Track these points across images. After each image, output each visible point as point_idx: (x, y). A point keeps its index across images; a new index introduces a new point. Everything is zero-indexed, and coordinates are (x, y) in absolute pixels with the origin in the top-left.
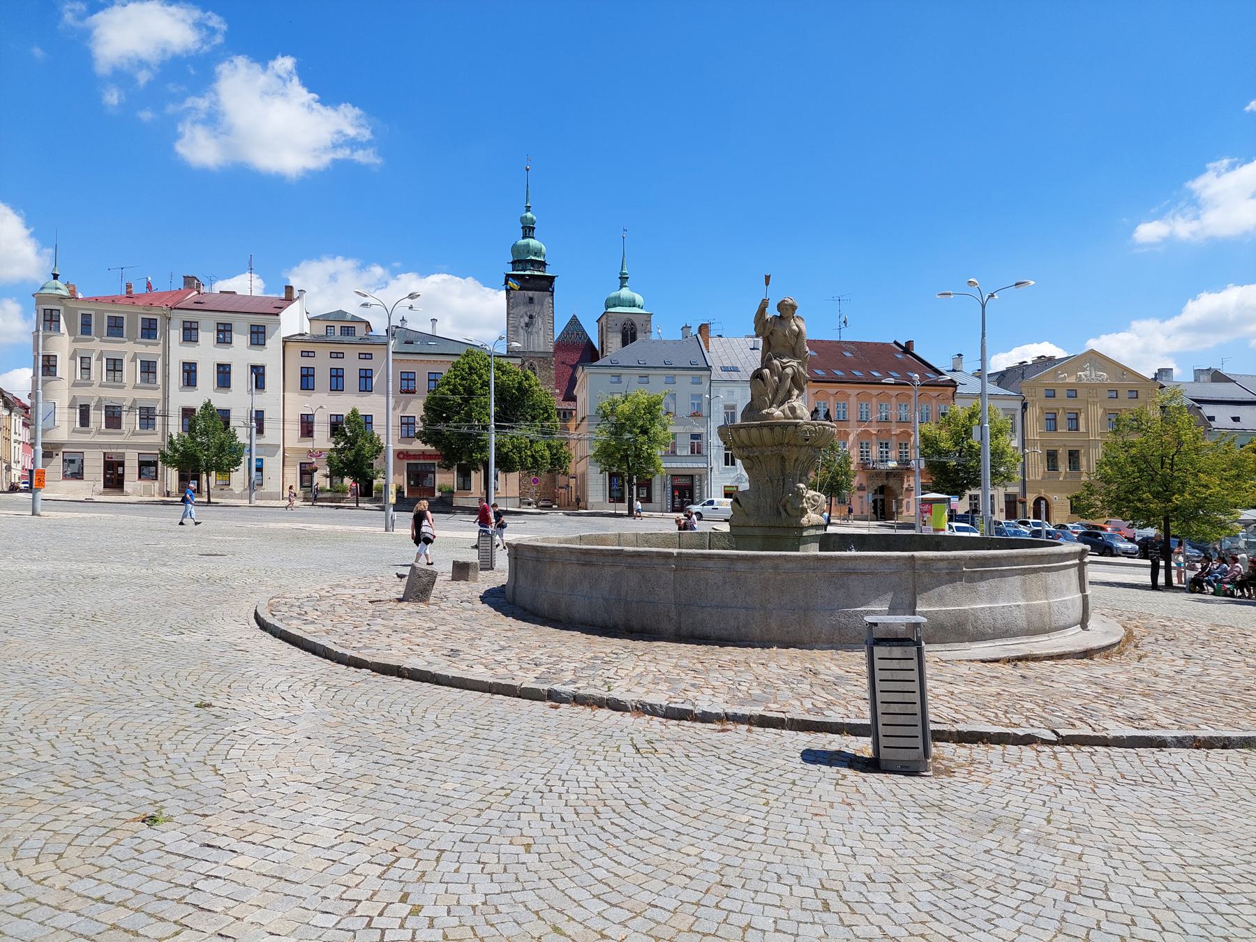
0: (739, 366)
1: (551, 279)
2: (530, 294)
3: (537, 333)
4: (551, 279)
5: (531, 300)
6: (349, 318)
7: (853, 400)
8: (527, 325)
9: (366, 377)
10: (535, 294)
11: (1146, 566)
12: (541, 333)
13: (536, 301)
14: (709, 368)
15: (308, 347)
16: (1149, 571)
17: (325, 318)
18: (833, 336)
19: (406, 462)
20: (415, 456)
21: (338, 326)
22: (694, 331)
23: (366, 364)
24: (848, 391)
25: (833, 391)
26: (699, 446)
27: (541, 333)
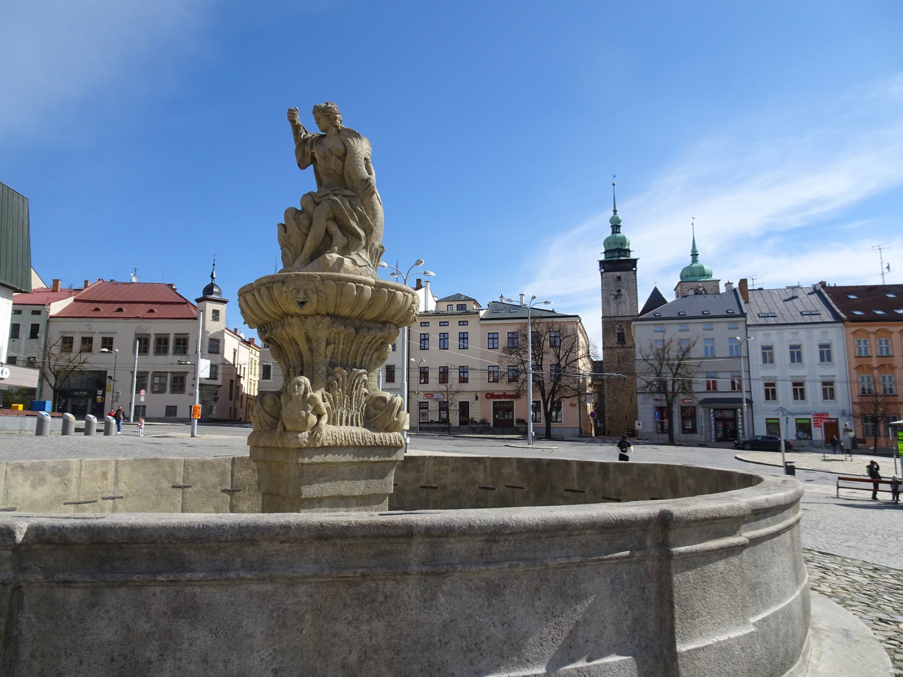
0: (777, 311)
1: (634, 262)
2: (618, 274)
3: (625, 302)
4: (634, 262)
5: (619, 278)
6: (463, 298)
7: (896, 337)
9: (464, 338)
12: (628, 302)
13: (623, 279)
14: (743, 315)
15: (425, 320)
16: (872, 492)
17: (447, 300)
18: (878, 282)
19: (492, 400)
20: (498, 397)
21: (455, 304)
22: (736, 285)
23: (463, 329)
24: (891, 329)
25: (874, 329)
27: (628, 302)
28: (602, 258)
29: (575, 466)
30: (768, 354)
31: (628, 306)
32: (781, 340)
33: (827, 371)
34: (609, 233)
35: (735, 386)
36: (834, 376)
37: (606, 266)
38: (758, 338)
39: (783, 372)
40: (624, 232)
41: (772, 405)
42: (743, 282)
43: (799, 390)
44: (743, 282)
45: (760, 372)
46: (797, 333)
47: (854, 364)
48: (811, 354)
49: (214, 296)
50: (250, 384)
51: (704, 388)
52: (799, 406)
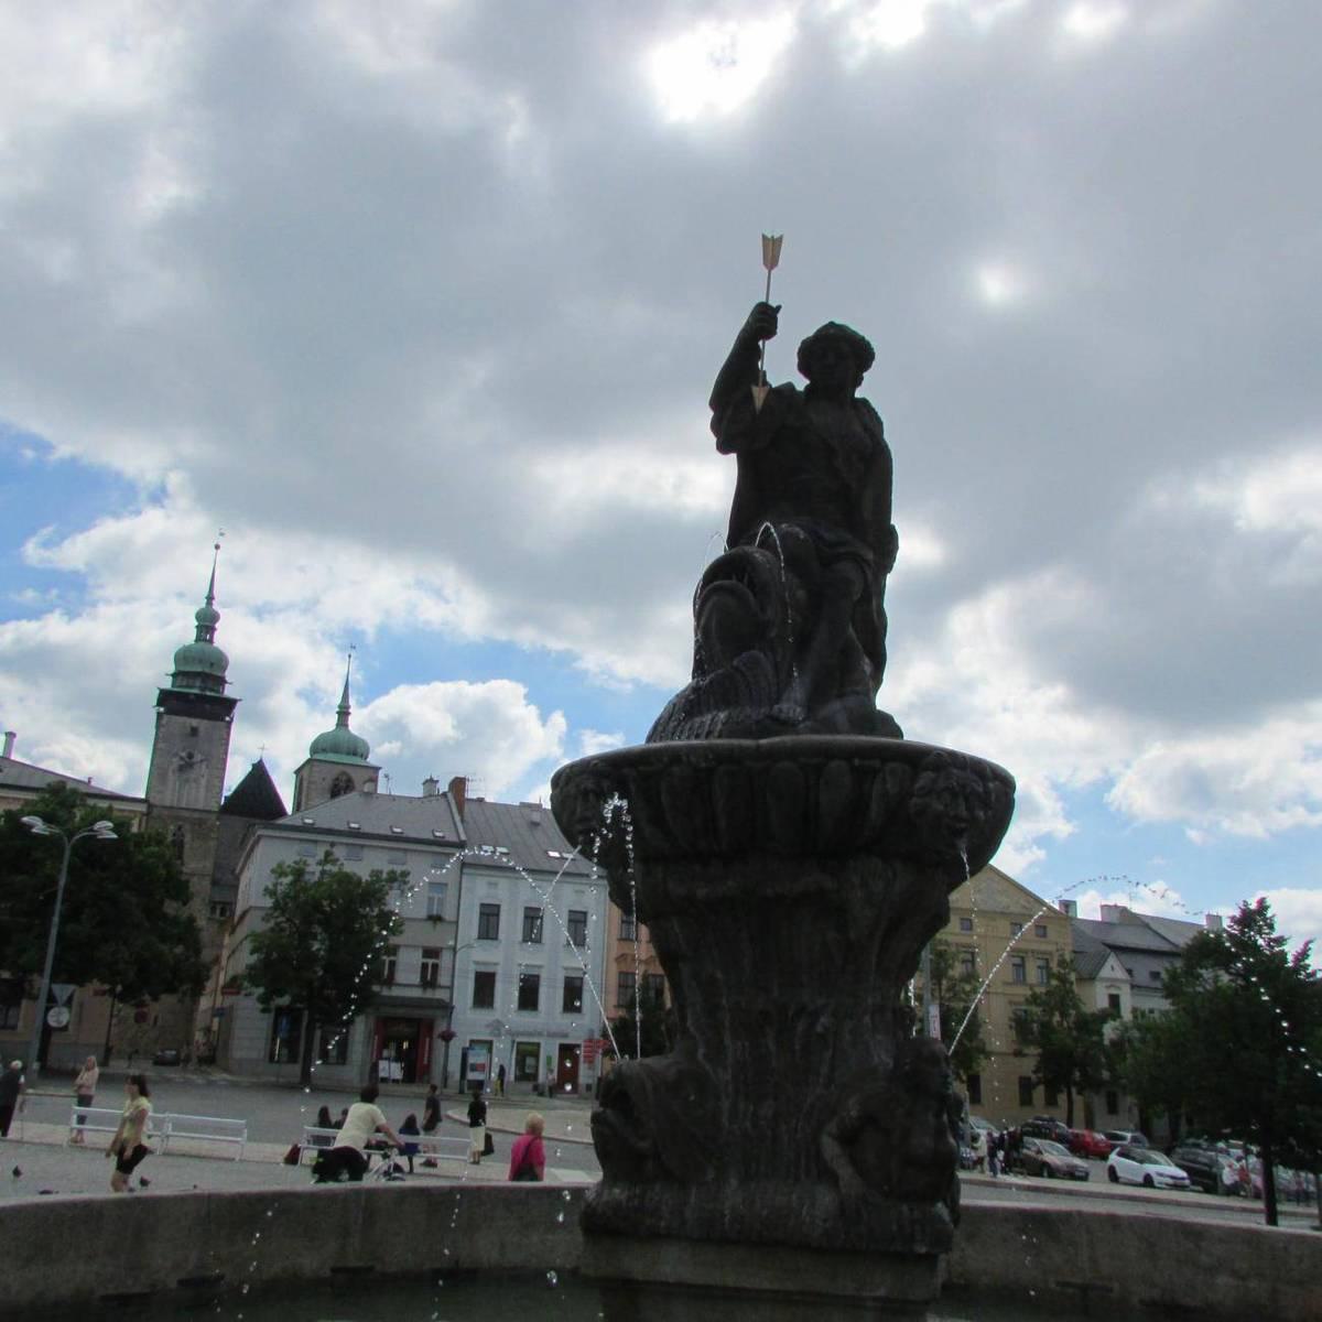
1: (230, 704)
2: (194, 722)
3: (196, 781)
4: (230, 704)
5: (194, 731)
8: (181, 769)
10: (203, 725)
11: (1253, 1211)
12: (203, 782)
22: (443, 787)
26: (435, 967)
27: (203, 782)
28: (167, 684)
29: (1045, 1174)
30: (490, 917)
31: (202, 790)
32: (513, 897)
33: (577, 960)
34: (190, 636)
35: (429, 979)
36: (540, 967)
37: (169, 701)
38: (479, 890)
39: (509, 957)
40: (223, 639)
41: (484, 1016)
42: (459, 785)
43: (529, 996)
44: (459, 785)
45: (473, 955)
46: (496, 884)
47: (614, 953)
48: (556, 926)
49: (1161, 966)
50: (376, 988)
51: (416, 979)
52: (527, 1020)
